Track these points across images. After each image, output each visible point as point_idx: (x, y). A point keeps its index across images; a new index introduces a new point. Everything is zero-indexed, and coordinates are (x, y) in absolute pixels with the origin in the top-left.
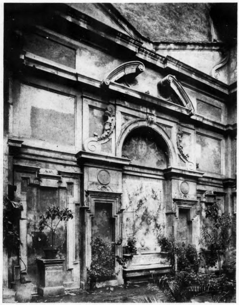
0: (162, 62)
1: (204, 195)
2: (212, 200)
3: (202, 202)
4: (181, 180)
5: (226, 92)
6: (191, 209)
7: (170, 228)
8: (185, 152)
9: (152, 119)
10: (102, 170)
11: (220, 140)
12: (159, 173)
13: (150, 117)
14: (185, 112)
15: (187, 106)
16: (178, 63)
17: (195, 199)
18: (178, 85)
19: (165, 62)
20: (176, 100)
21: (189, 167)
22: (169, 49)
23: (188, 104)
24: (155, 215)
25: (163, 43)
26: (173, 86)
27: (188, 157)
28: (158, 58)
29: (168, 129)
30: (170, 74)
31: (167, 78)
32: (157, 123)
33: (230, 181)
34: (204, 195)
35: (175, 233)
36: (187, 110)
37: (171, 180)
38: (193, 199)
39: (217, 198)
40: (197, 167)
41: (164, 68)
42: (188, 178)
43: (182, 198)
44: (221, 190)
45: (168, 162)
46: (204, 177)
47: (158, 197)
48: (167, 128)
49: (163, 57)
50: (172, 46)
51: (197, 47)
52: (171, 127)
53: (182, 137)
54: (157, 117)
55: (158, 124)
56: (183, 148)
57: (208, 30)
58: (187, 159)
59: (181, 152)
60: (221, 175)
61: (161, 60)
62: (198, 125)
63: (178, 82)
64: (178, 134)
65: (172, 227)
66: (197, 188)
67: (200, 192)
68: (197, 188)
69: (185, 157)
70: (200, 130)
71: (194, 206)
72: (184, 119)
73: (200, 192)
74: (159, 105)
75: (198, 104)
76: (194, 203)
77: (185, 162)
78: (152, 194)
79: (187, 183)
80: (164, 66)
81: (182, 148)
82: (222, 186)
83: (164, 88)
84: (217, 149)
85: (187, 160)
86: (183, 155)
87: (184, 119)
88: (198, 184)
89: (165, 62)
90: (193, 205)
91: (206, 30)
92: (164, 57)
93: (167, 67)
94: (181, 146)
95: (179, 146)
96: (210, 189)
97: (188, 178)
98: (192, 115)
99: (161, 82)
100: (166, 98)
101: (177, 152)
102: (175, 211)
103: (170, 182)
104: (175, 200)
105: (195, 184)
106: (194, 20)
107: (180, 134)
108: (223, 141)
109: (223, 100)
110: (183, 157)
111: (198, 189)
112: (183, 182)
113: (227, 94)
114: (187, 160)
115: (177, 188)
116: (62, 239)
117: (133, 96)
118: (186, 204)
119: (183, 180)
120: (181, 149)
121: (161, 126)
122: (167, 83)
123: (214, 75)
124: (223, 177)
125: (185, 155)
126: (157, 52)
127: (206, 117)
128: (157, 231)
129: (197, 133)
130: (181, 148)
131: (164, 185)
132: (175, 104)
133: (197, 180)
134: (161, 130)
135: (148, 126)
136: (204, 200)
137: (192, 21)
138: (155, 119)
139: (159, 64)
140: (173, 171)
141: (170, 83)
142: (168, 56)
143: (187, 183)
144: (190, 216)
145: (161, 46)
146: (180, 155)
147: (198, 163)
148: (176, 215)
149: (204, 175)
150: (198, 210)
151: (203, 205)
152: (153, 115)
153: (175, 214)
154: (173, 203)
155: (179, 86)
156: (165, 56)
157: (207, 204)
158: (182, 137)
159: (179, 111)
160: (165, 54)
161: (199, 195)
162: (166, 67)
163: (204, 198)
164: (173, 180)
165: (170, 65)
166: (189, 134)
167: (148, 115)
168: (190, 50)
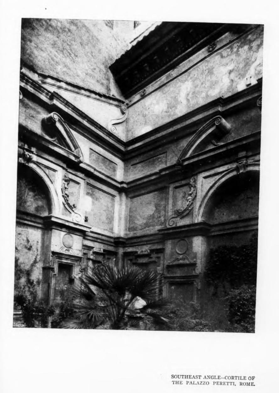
0: (48, 97)
1: (91, 252)
2: (100, 259)
3: (89, 259)
4: (64, 232)
5: (122, 148)
6: (74, 265)
7: (46, 285)
8: (72, 201)
9: (30, 156)
10: (66, 234)
11: (113, 196)
12: (39, 221)
13: (27, 153)
14: (73, 158)
15: (75, 151)
16: (67, 104)
17: (80, 255)
18: (65, 126)
19: (51, 98)
20: (62, 141)
21: (76, 218)
22: (59, 87)
23: (76, 150)
24: (27, 268)
25: (52, 78)
26: (58, 125)
27: (75, 207)
28: (43, 92)
29: (52, 172)
30: (54, 111)
31: (52, 114)
32: (37, 162)
33: (121, 240)
34: (91, 252)
35: (52, 291)
36: (74, 156)
37: (51, 229)
38: (78, 254)
39: (107, 257)
40: (86, 220)
41: (50, 104)
42: (71, 230)
43: (64, 253)
44: (111, 248)
45: (50, 210)
46: (92, 232)
47: (34, 248)
48: (50, 170)
49: (49, 92)
50: (63, 85)
51: (93, 95)
52: (55, 170)
53: (68, 184)
54: (38, 155)
55: (37, 164)
56: (69, 197)
57: (107, 83)
58: (74, 209)
59: (66, 201)
60: (113, 233)
61: (47, 94)
62: (88, 174)
63: (64, 122)
64: (63, 179)
65: (47, 285)
66: (83, 243)
67: (85, 247)
68: (83, 243)
69: (70, 206)
70: (92, 182)
71: (78, 262)
72: (73, 165)
73: (85, 247)
74: (47, 145)
75: (90, 154)
76: (78, 259)
77: (71, 213)
78: (26, 244)
79: (71, 236)
80: (51, 103)
81: (68, 196)
82: (40, 226)
83: (48, 125)
84: (110, 205)
85: (73, 211)
86: (68, 204)
87: (73, 165)
88: (84, 238)
89: (51, 98)
90: (77, 261)
91: (105, 82)
92: (50, 92)
93: (54, 105)
94: (66, 194)
95: (64, 193)
96: (98, 247)
97: (71, 230)
98: (81, 162)
99: (46, 118)
100: (52, 138)
101: (62, 200)
102: (53, 266)
103: (50, 232)
104: (54, 253)
105: (81, 238)
106: (92, 67)
107: (66, 181)
108: (117, 198)
109: (120, 157)
110: (70, 207)
111: (84, 244)
112: (66, 234)
113: (122, 151)
114: (73, 211)
115: (58, 241)
116: (174, 304)
117: (59, 152)
118: (68, 259)
119: (66, 232)
120: (66, 197)
121: (42, 167)
122: (51, 119)
123: (110, 128)
124: (116, 236)
125: (71, 204)
126: (44, 86)
127: (97, 169)
128: (29, 288)
129: (88, 184)
130: (66, 196)
131: (43, 235)
132: (63, 147)
133: (83, 234)
134: (42, 172)
135: (24, 164)
136: (92, 257)
137: (90, 68)
138: (35, 158)
139: (43, 97)
140: (53, 219)
141: (55, 122)
142: (54, 92)
143: (71, 236)
144: (72, 273)
145: (49, 80)
146: (65, 203)
147: (87, 216)
148: (54, 270)
149: (91, 230)
150: (83, 267)
151: (90, 263)
152: (32, 152)
153: (53, 269)
154: (52, 256)
155: (67, 128)
156: (52, 91)
157: (94, 262)
158: (68, 184)
159: (65, 154)
160: (52, 89)
161: (85, 251)
162: (52, 103)
163: (92, 255)
164: (53, 230)
165: (56, 102)
166: (78, 183)
167: (25, 151)
168: (85, 95)
